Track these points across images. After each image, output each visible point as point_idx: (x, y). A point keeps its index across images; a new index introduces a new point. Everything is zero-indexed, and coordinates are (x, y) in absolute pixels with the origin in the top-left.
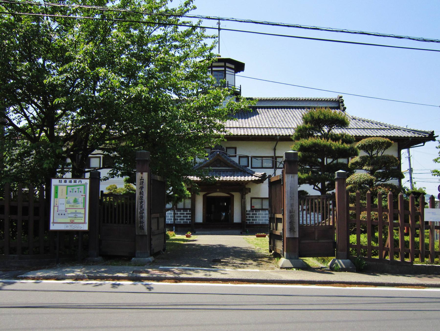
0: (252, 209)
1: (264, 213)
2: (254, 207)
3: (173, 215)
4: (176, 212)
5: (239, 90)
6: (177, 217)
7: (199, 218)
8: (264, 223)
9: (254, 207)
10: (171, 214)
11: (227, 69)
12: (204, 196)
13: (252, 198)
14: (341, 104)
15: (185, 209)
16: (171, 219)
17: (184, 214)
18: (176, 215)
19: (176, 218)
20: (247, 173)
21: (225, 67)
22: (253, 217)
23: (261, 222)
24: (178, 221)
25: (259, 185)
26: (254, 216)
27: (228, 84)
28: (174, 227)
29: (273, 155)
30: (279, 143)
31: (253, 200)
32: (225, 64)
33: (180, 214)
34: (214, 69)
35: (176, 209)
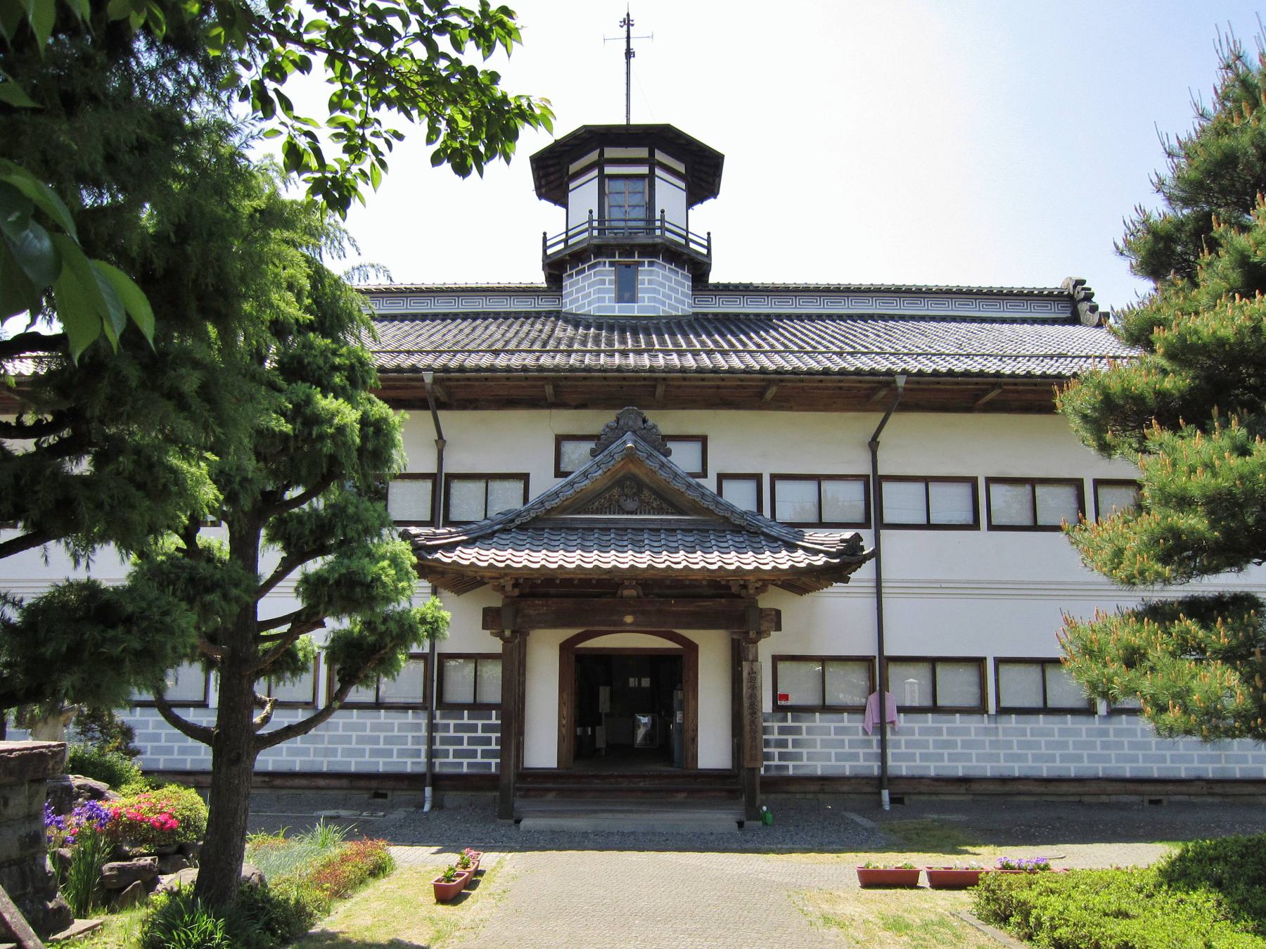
0: (780, 709)
1: (832, 725)
2: (786, 697)
3: (424, 733)
4: (438, 720)
5: (704, 251)
6: (445, 741)
7: (543, 748)
8: (917, 773)
9: (786, 697)
10: (417, 727)
11: (658, 172)
12: (566, 648)
13: (776, 659)
14: (1084, 307)
15: (478, 708)
16: (417, 753)
17: (473, 728)
18: (438, 735)
19: (438, 746)
20: (767, 536)
21: (651, 163)
22: (1105, 746)
23: (819, 768)
24: (449, 763)
25: (807, 597)
26: (790, 738)
27: (662, 220)
28: (428, 790)
29: (866, 469)
30: (895, 418)
31: (781, 666)
32: (652, 154)
33: (458, 728)
34: (609, 170)
35: (441, 704)
